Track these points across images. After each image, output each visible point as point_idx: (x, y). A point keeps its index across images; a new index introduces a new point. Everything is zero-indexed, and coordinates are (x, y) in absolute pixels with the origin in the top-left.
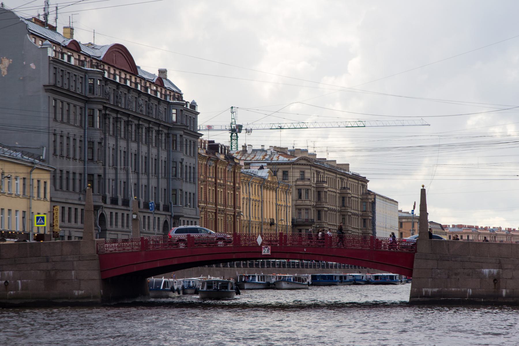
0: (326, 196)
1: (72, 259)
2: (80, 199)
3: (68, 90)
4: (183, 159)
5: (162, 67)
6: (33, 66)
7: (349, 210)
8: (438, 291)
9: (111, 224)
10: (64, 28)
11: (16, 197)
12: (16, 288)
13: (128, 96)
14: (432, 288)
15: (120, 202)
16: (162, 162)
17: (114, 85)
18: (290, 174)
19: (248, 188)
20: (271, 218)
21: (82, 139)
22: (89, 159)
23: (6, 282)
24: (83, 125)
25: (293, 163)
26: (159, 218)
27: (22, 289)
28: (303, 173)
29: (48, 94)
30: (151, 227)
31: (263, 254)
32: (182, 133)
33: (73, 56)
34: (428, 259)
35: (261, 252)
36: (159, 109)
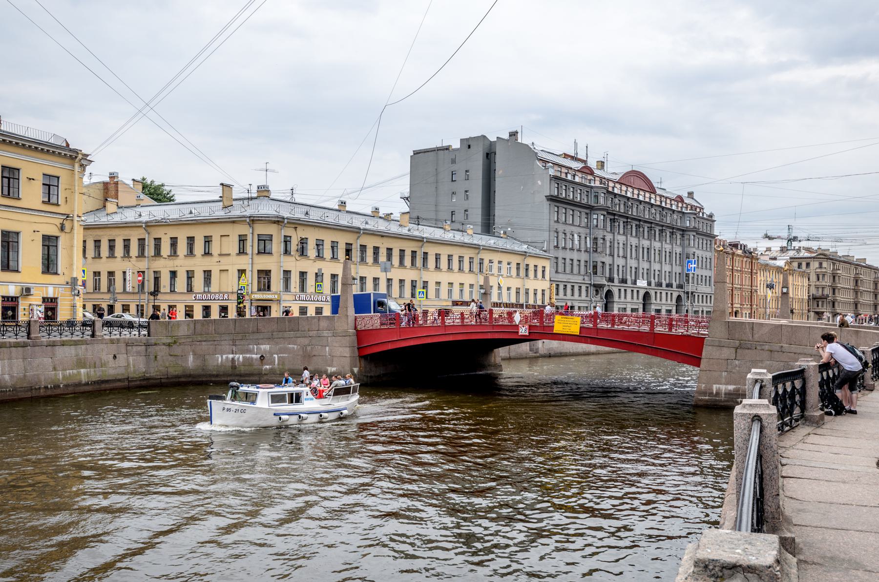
0: (839, 279)
1: (326, 335)
2: (584, 279)
3: (619, 212)
4: (694, 252)
5: (690, 190)
6: (539, 183)
7: (861, 288)
8: (735, 390)
10: (597, 162)
12: (273, 363)
14: (727, 384)
15: (664, 285)
16: (643, 251)
18: (811, 264)
19: (765, 273)
21: (625, 242)
22: (593, 251)
23: (262, 356)
24: (589, 226)
25: (814, 258)
26: (671, 294)
27: (278, 364)
28: (821, 264)
29: (549, 202)
31: (520, 334)
32: (695, 234)
34: (723, 346)
35: (518, 332)
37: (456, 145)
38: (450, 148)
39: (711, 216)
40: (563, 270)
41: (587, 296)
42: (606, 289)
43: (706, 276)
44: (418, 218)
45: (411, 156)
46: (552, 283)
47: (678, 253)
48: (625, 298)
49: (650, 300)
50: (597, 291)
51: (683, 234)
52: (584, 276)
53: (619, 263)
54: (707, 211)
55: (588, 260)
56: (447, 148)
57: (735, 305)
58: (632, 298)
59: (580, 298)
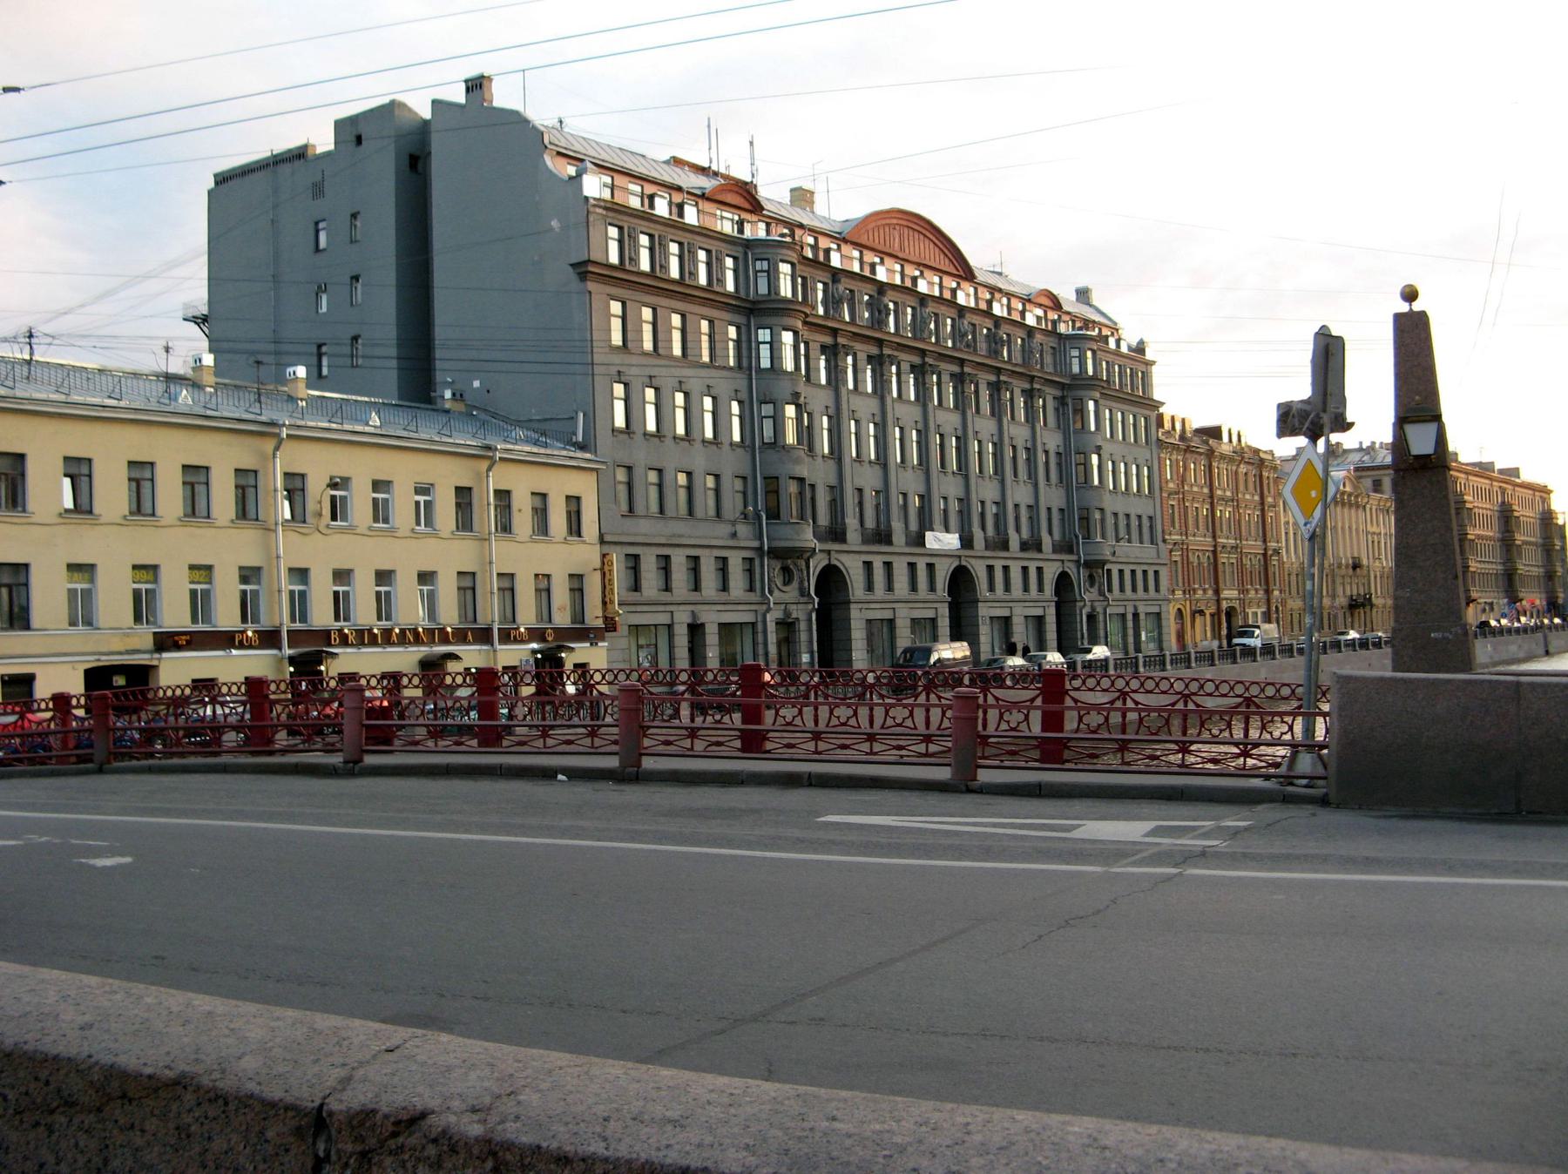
2: (734, 535)
5: (1080, 285)
9: (992, 588)
11: (127, 523)
13: (921, 314)
17: (953, 310)
20: (1356, 555)
24: (745, 363)
30: (997, 585)
33: (961, 289)
36: (1029, 346)
37: (324, 142)
38: (310, 152)
39: (1140, 349)
40: (1155, 556)
41: (751, 589)
42: (817, 564)
43: (1139, 517)
44: (31, 336)
45: (210, 192)
46: (606, 549)
47: (1052, 448)
48: (890, 587)
49: (974, 590)
50: (786, 570)
51: (1063, 398)
52: (734, 523)
53: (860, 483)
54: (1130, 338)
55: (747, 472)
56: (300, 155)
57: (1226, 594)
58: (1026, 589)
59: (932, 597)
